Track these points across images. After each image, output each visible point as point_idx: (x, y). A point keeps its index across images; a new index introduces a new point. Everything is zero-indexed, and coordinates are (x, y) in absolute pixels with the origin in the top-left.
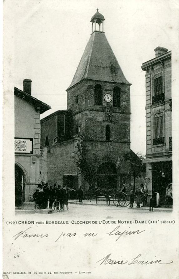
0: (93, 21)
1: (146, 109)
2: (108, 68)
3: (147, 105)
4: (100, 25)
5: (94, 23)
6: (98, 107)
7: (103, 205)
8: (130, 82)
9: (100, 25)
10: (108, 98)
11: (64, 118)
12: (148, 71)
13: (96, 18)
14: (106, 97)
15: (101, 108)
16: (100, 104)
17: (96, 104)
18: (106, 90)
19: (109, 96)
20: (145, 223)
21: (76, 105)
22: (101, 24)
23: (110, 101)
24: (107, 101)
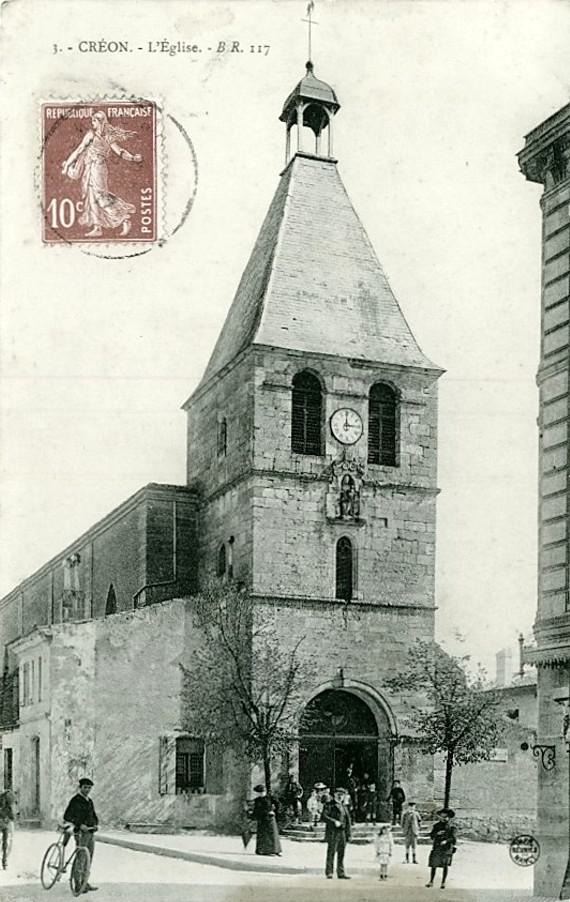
0: (289, 116)
1: (538, 385)
2: (350, 304)
3: (545, 357)
4: (317, 133)
5: (294, 127)
6: (308, 464)
7: (10, 762)
8: (433, 357)
9: (317, 133)
10: (347, 426)
11: (177, 519)
12: (558, 169)
13: (306, 100)
14: (338, 421)
15: (317, 465)
16: (317, 451)
17: (297, 448)
18: (341, 396)
19: (353, 420)
20: (340, 877)
21: (220, 460)
22: (324, 132)
23: (356, 437)
24: (343, 440)
